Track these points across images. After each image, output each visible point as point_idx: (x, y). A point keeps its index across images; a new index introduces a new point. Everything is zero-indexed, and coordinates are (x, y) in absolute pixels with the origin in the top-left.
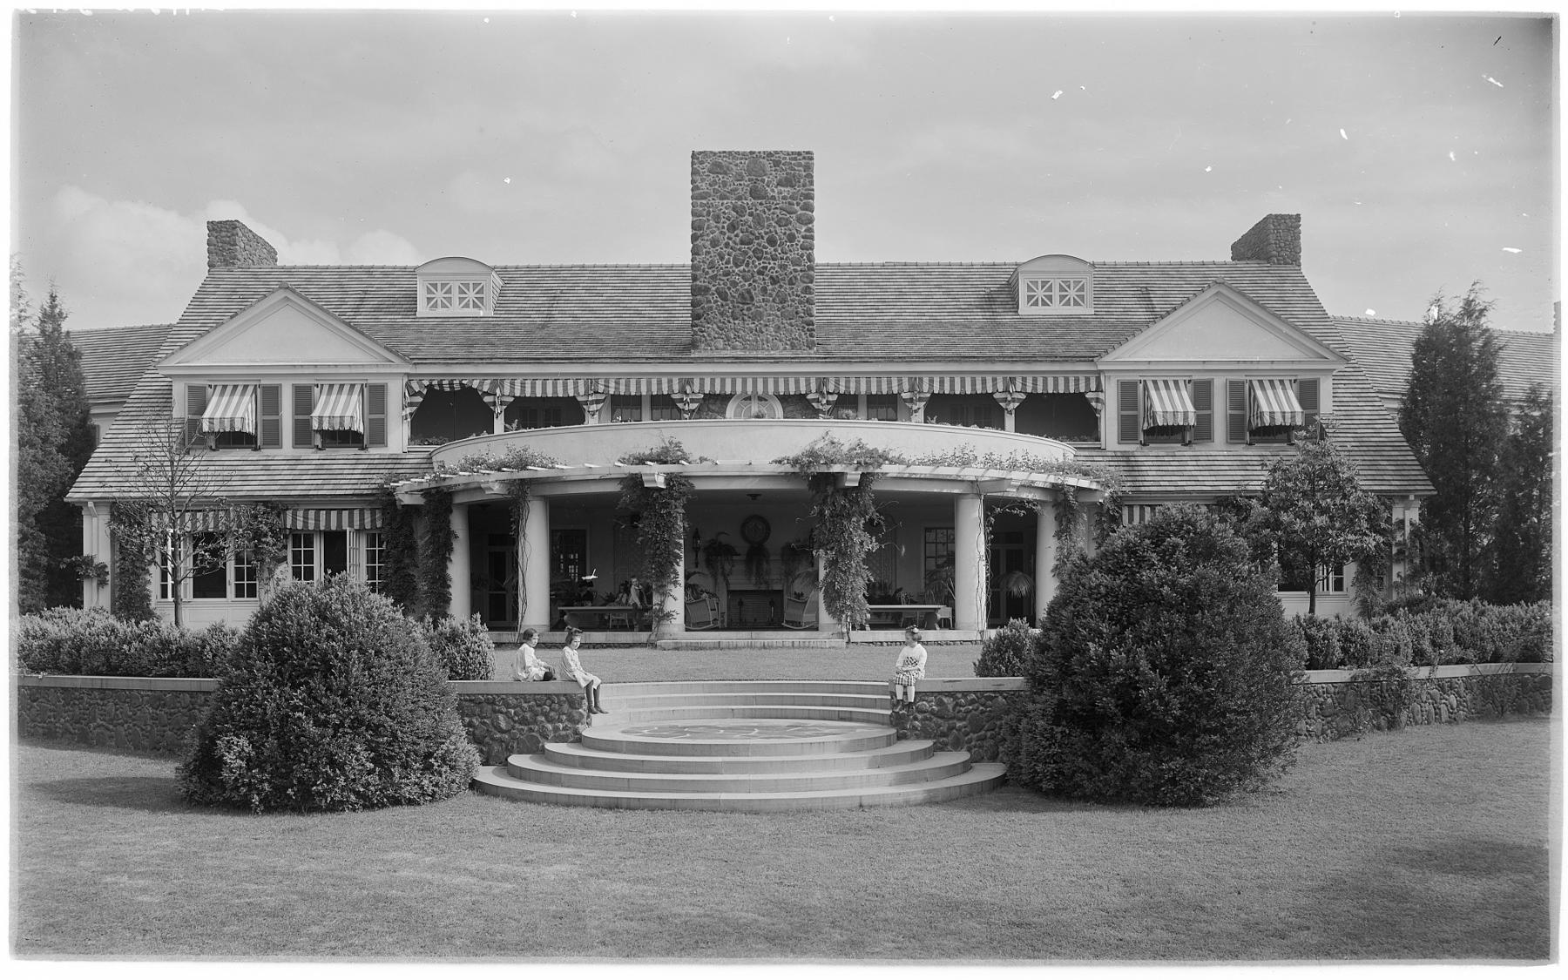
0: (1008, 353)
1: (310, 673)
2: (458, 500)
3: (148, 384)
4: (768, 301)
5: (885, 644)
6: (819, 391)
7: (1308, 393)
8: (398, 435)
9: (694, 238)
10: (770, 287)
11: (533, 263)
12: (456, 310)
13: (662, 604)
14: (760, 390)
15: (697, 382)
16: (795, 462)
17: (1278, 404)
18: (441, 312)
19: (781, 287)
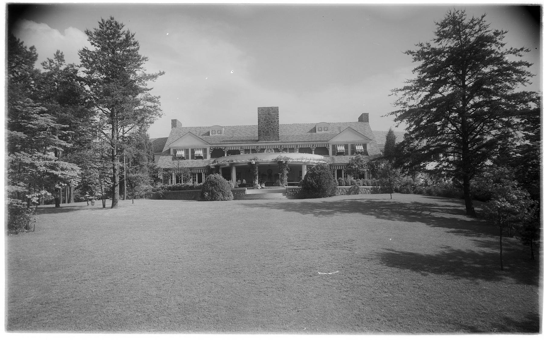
0: (313, 140)
1: (215, 185)
2: (221, 167)
3: (165, 149)
6: (280, 148)
7: (365, 146)
8: (209, 156)
9: (258, 122)
11: (229, 126)
12: (217, 135)
13: (255, 182)
15: (259, 147)
16: (275, 159)
17: (359, 148)
18: (214, 135)
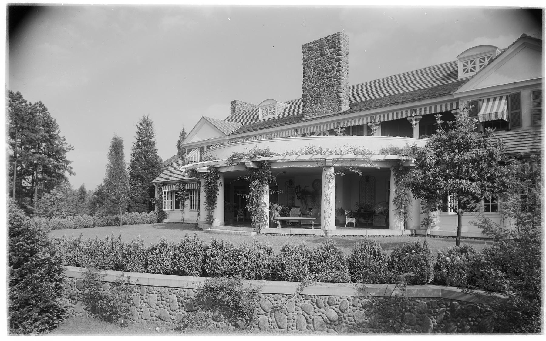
4: (325, 95)
5: (275, 235)
10: (326, 89)
14: (308, 132)
19: (330, 88)
